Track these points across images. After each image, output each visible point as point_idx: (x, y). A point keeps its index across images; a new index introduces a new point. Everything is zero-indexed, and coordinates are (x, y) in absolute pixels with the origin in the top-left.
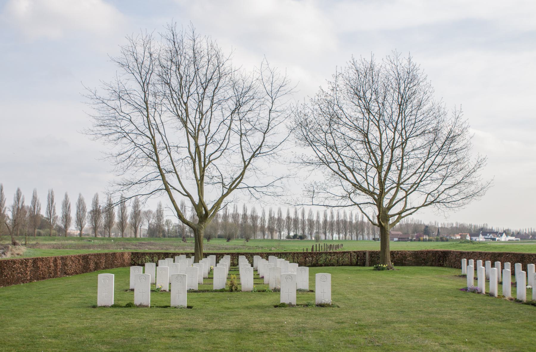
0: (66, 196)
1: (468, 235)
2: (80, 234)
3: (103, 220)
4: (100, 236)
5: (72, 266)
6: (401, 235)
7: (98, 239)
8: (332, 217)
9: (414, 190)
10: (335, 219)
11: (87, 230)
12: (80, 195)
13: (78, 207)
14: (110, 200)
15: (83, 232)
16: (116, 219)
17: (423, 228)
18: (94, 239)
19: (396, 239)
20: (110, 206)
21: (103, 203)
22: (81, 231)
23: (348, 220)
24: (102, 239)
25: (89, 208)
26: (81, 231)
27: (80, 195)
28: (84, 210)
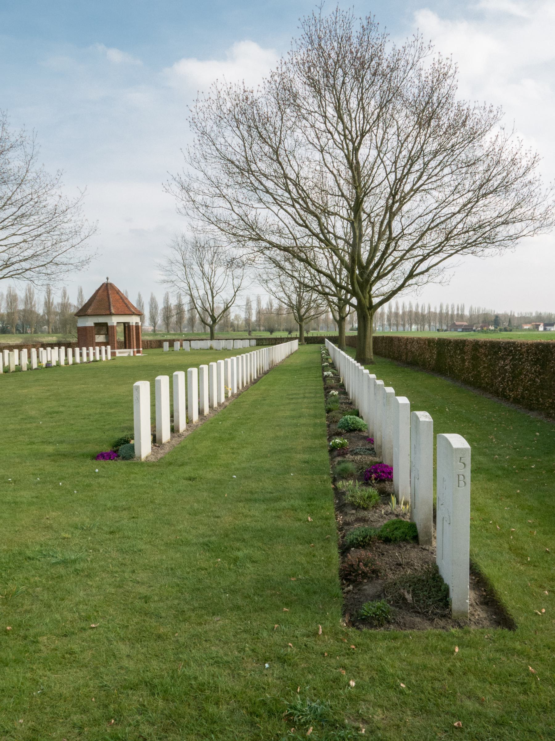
0: (140, 296)
1: (542, 325)
2: (154, 331)
3: (174, 319)
4: (172, 332)
5: (154, 345)
6: (465, 326)
7: (171, 334)
8: (397, 308)
9: (213, 297)
10: (455, 313)
11: (160, 326)
12: (152, 294)
13: (151, 306)
14: (180, 301)
15: (156, 328)
16: (187, 316)
17: (493, 318)
18: (166, 335)
19: (460, 330)
20: (179, 307)
21: (173, 302)
22: (154, 327)
23: (420, 311)
24: (174, 335)
25: (161, 306)
26: (154, 327)
27: (152, 294)
28: (156, 308)
